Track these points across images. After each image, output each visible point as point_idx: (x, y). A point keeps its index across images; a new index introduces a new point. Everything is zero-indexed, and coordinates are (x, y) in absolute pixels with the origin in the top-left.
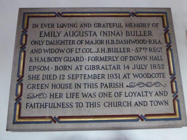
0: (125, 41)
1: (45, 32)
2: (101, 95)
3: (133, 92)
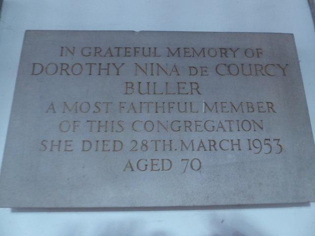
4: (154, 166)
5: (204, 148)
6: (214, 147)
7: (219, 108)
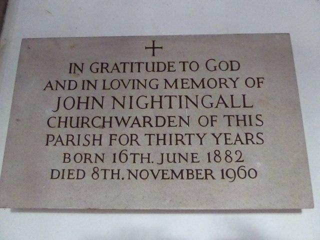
0: (88, 137)
1: (192, 79)
2: (250, 82)
3: (89, 127)
4: (199, 175)
5: (241, 141)
6: (90, 160)
7: (66, 176)
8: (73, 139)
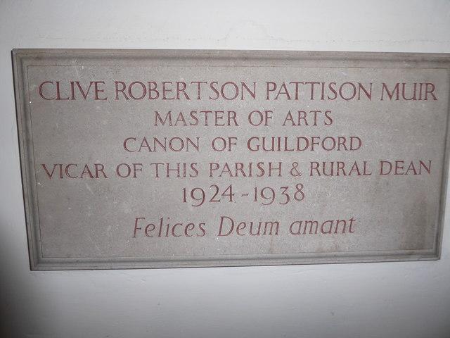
8: (433, 90)
